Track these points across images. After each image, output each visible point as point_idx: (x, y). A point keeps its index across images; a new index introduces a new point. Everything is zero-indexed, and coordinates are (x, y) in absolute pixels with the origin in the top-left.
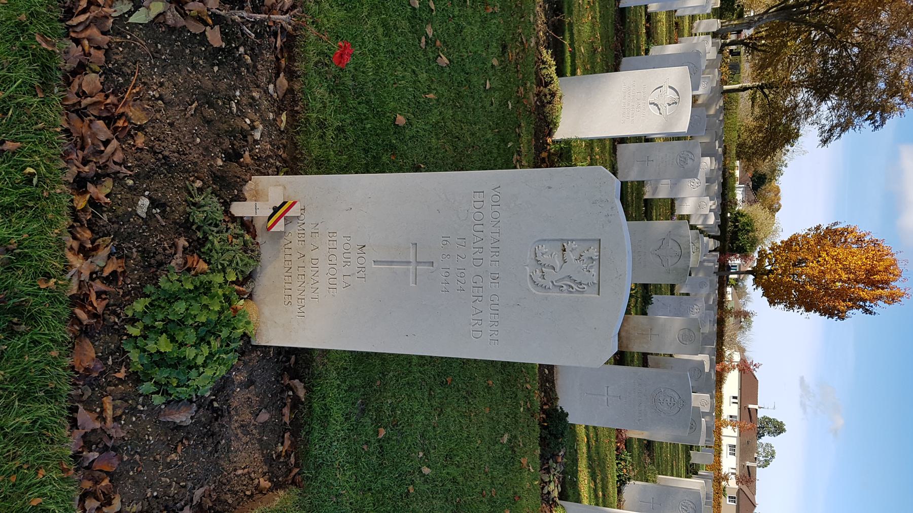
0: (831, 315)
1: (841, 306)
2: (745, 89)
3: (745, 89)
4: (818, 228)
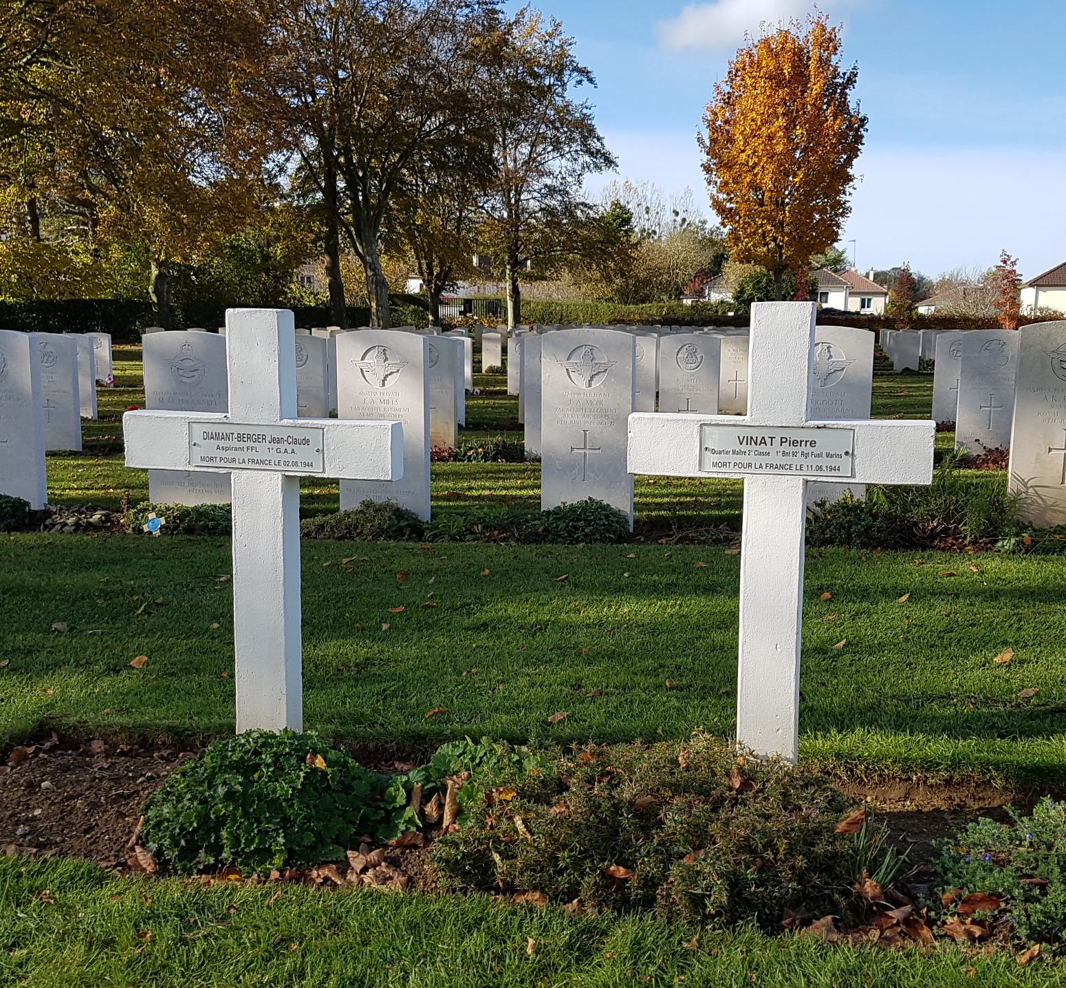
0: (858, 139)
1: (835, 125)
2: (515, 292)
3: (515, 292)
4: (707, 169)
